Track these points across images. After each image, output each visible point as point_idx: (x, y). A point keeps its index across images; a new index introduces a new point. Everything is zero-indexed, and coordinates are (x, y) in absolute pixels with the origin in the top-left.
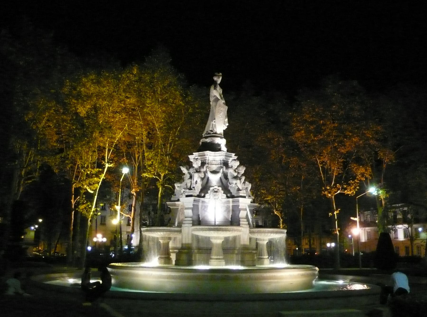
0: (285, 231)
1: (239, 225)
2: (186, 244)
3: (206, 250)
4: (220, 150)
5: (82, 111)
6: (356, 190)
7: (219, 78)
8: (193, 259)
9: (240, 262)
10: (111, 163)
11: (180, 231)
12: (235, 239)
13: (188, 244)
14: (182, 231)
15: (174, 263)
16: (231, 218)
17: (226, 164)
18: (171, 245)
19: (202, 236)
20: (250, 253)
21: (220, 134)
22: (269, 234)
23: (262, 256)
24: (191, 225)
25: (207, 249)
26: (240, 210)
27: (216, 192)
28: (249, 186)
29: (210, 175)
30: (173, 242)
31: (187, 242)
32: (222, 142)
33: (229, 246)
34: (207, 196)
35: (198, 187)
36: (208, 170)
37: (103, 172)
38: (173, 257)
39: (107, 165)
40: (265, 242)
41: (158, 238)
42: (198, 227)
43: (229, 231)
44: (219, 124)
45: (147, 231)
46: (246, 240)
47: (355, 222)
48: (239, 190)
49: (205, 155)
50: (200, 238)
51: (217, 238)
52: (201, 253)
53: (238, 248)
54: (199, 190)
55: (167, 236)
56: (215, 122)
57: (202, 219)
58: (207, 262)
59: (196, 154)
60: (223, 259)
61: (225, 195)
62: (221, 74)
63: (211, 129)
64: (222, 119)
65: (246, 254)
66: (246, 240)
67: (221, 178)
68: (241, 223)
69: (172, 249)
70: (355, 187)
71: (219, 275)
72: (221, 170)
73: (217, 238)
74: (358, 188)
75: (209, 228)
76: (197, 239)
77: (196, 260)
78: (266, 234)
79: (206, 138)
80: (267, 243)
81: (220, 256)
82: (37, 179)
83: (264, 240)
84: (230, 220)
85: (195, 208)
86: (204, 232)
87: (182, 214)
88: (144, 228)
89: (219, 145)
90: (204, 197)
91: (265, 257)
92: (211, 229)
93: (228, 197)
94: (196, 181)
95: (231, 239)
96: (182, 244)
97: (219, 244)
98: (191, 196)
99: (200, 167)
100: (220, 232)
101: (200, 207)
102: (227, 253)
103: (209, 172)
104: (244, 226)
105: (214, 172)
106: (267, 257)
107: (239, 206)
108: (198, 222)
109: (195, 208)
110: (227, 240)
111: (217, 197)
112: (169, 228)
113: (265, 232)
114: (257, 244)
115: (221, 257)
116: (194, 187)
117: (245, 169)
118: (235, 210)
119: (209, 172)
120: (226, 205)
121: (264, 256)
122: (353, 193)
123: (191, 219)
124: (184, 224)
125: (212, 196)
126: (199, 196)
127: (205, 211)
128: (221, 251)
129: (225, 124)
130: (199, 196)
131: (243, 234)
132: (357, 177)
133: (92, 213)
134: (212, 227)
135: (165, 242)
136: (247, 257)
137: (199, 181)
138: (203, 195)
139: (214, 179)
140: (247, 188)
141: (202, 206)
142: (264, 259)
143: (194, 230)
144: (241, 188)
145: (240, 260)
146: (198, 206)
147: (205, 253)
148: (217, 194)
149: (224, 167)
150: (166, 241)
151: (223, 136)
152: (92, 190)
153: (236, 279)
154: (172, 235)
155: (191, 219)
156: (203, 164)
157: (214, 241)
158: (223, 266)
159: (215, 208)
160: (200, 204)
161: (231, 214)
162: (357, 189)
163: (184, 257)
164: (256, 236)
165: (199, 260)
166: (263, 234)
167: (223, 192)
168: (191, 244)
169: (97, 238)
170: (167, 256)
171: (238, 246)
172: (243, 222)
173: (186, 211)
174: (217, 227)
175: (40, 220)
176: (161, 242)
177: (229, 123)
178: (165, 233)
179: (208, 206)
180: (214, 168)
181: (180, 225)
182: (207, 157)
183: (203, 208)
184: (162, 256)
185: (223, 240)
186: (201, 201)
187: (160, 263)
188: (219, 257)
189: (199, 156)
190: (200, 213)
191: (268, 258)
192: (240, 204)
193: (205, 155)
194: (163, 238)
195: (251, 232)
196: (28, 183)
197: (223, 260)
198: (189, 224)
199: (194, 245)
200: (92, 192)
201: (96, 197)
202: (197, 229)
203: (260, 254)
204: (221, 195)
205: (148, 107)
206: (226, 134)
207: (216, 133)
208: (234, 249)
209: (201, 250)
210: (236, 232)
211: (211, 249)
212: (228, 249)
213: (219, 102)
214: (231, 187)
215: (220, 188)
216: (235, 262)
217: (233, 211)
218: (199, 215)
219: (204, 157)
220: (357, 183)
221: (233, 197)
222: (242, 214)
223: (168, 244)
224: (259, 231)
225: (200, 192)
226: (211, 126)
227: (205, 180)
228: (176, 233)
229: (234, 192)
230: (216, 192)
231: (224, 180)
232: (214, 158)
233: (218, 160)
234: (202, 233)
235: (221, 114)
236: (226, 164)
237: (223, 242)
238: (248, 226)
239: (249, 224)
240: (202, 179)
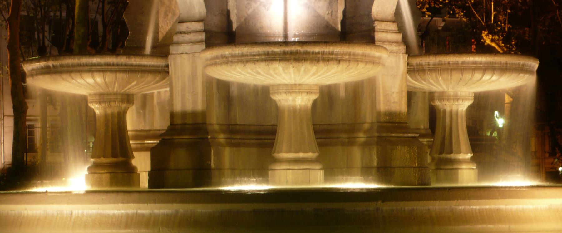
0: (535, 64)
2: (184, 115)
3: (256, 130)
8: (213, 165)
9: (374, 171)
11: (164, 72)
12: (357, 92)
13: (194, 114)
14: (171, 70)
15: (144, 182)
16: (343, 22)
18: (132, 123)
19: (242, 86)
22: (477, 75)
23: (451, 152)
24: (204, 46)
25: (259, 133)
30: (139, 113)
31: (189, 107)
33: (339, 116)
38: (142, 163)
40: (463, 106)
41: (84, 99)
42: (227, 51)
43: (339, 61)
45: (47, 71)
46: (395, 97)
50: (234, 91)
51: (295, 86)
53: (366, 126)
55: (116, 88)
57: (240, 27)
58: (261, 171)
66: (395, 97)
68: (378, 36)
69: (136, 138)
73: (295, 86)
75: (268, 54)
76: (224, 91)
77: (220, 168)
78: (467, 76)
81: (306, 152)
83: (456, 98)
84: (339, 27)
86: (250, 66)
87: (166, 15)
88: (32, 61)
90: (10, 21)
91: (461, 156)
92: (274, 54)
96: (172, 115)
97: (303, 110)
100: (304, 67)
106: (469, 156)
110: (327, 95)
112: (122, 60)
113: (462, 69)
114: (434, 115)
115: (310, 155)
121: (459, 152)
123: (199, 26)
124: (178, 43)
128: (308, 134)
131: (385, 73)
134: (277, 49)
135: (109, 111)
136: (402, 155)
143: (214, 62)
145: (375, 163)
150: (114, 108)
154: (137, 86)
155: (199, 26)
157: (285, 100)
158: (317, 180)
163: (181, 159)
166: (456, 76)
168: (204, 114)
170: (120, 159)
171: (368, 118)
172: (385, 33)
174: (290, 51)
176: (97, 112)
178: (109, 77)
181: (162, 49)
184: (103, 160)
185: (314, 97)
188: (301, 155)
191: (473, 160)
194: (103, 98)
195: (411, 70)
197: (318, 166)
198: (195, 42)
199: (215, 119)
202: (223, 57)
208: (352, 128)
209: (236, 134)
210: (361, 66)
212: (333, 127)
218: (228, 13)
223: (121, 118)
224: (440, 64)
228: (149, 78)
234: (245, 74)
237: (315, 103)
238: (403, 48)
239: (405, 41)
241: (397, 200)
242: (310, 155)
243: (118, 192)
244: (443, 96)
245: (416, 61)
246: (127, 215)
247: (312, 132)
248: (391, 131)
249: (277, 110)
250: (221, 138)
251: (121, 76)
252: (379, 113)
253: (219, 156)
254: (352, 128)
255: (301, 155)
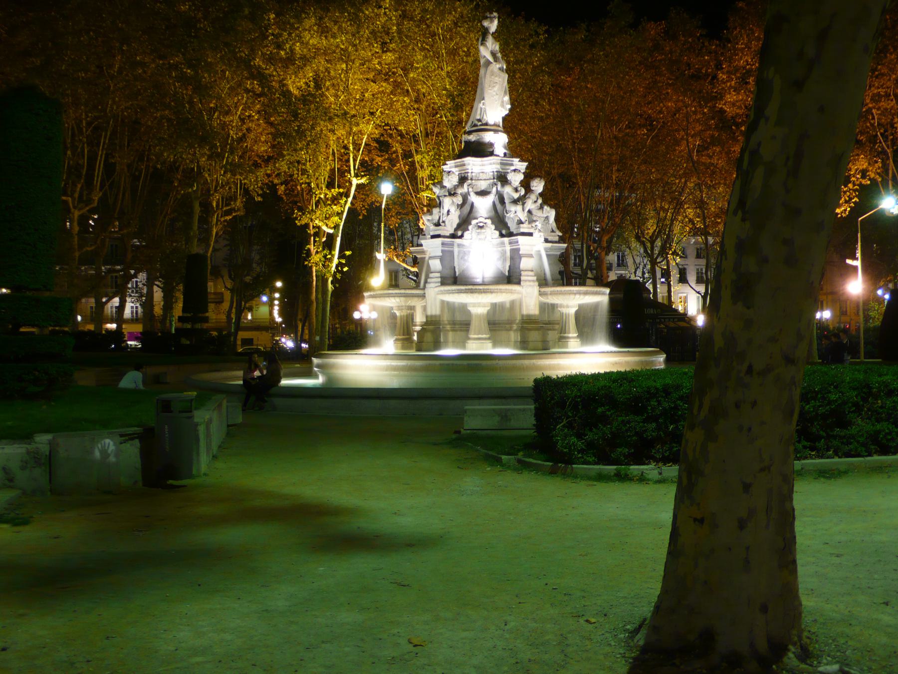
0: (608, 291)
1: (519, 283)
2: (431, 316)
3: (462, 324)
4: (492, 154)
5: (296, 84)
6: (852, 205)
7: (492, 22)
10: (362, 176)
11: (423, 296)
13: (435, 316)
17: (502, 179)
20: (541, 331)
21: (495, 125)
26: (520, 257)
27: (481, 227)
28: (552, 214)
29: (473, 198)
31: (434, 313)
32: (499, 141)
34: (466, 234)
35: (452, 221)
36: (470, 190)
39: (355, 181)
40: (572, 311)
41: (392, 308)
43: (492, 292)
44: (494, 106)
47: (856, 268)
48: (520, 222)
49: (464, 165)
51: (478, 305)
54: (455, 226)
59: (451, 163)
60: (489, 339)
61: (497, 233)
63: (478, 117)
64: (496, 97)
68: (522, 278)
70: (851, 199)
72: (494, 189)
73: (478, 305)
79: (470, 133)
82: (241, 213)
83: (568, 307)
89: (491, 145)
90: (461, 237)
91: (570, 335)
93: (502, 235)
94: (448, 211)
95: (508, 305)
98: (438, 236)
99: (456, 187)
100: (476, 295)
101: (456, 254)
102: (495, 330)
103: (472, 194)
104: (528, 283)
105: (483, 193)
106: (576, 335)
107: (518, 250)
108: (454, 279)
109: (447, 257)
110: (495, 308)
111: (482, 236)
112: (403, 291)
113: (571, 293)
115: (484, 336)
116: (444, 222)
118: (515, 256)
119: (472, 194)
120: (500, 249)
122: (845, 210)
123: (438, 275)
125: (474, 235)
126: (453, 236)
128: (485, 326)
129: (503, 106)
130: (453, 236)
131: (528, 297)
132: (853, 179)
133: (333, 269)
137: (453, 209)
138: (460, 233)
139: (483, 206)
140: (547, 218)
141: (459, 252)
142: (568, 338)
143: (443, 293)
144: (523, 220)
146: (452, 252)
148: (483, 231)
149: (499, 184)
152: (331, 228)
156: (463, 179)
159: (482, 254)
160: (456, 250)
161: (508, 264)
162: (854, 203)
163: (429, 337)
164: (551, 300)
167: (493, 227)
169: (361, 312)
173: (431, 262)
175: (279, 284)
179: (469, 252)
180: (483, 185)
182: (469, 167)
183: (461, 255)
186: (456, 245)
187: (397, 348)
188: (480, 336)
189: (456, 166)
190: (456, 264)
192: (521, 247)
193: (464, 165)
194: (400, 308)
195: (541, 294)
199: (446, 318)
200: (331, 231)
203: (563, 330)
204: (491, 232)
205: (418, 68)
206: (509, 125)
207: (486, 124)
212: (496, 324)
213: (491, 67)
214: (509, 218)
215: (489, 222)
216: (512, 343)
217: (512, 258)
219: (465, 167)
220: (855, 191)
221: (511, 234)
222: (526, 264)
225: (456, 230)
226: (479, 112)
227: (467, 208)
228: (416, 299)
229: (513, 227)
230: (481, 227)
231: (499, 206)
235: (496, 89)
236: (502, 179)
237: (488, 312)
240: (461, 207)
242: (484, 336)
243: (628, 352)
244: (562, 306)
245: (543, 290)
247: (486, 325)
248: (529, 324)
252: (523, 316)
253: (446, 337)
254: (510, 322)
255: (480, 336)
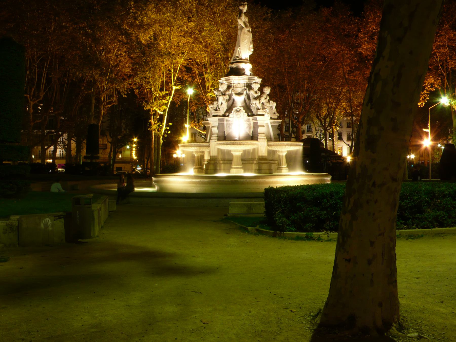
0: (302, 144)
1: (257, 139)
2: (213, 156)
3: (228, 160)
4: (244, 74)
5: (144, 38)
6: (426, 101)
7: (244, 7)
10: (178, 85)
11: (209, 146)
13: (215, 156)
16: (252, 134)
20: (268, 164)
21: (245, 59)
26: (258, 127)
27: (238, 111)
28: (274, 105)
29: (234, 97)
31: (214, 155)
32: (247, 67)
34: (231, 115)
35: (224, 108)
36: (233, 92)
37: (170, 95)
39: (174, 88)
40: (284, 154)
41: (193, 152)
43: (243, 144)
44: (245, 50)
47: (427, 133)
48: (258, 109)
49: (230, 80)
51: (237, 151)
52: (225, 164)
54: (225, 111)
56: (240, 49)
57: (227, 135)
58: (229, 171)
60: (242, 168)
61: (246, 114)
62: (246, 3)
63: (237, 56)
65: (263, 163)
67: (245, 99)
68: (259, 137)
70: (425, 98)
71: (230, 180)
72: (245, 92)
73: (237, 151)
74: (428, 98)
79: (233, 63)
80: (286, 155)
83: (282, 152)
85: (221, 126)
89: (243, 70)
90: (228, 116)
91: (283, 166)
93: (249, 116)
94: (222, 103)
98: (216, 116)
99: (225, 91)
102: (245, 164)
103: (234, 94)
104: (262, 140)
105: (239, 94)
108: (224, 137)
109: (221, 126)
113: (283, 145)
115: (239, 167)
116: (219, 109)
117: (270, 89)
119: (234, 94)
122: (422, 104)
123: (216, 135)
126: (224, 116)
127: (230, 128)
129: (249, 50)
130: (224, 116)
131: (262, 147)
138: (227, 114)
139: (239, 100)
141: (227, 124)
142: (282, 168)
144: (260, 108)
146: (223, 124)
147: (228, 164)
148: (239, 113)
149: (247, 89)
151: (249, 61)
152: (162, 111)
153: (243, 183)
156: (229, 87)
159: (238, 125)
160: (225, 123)
162: (427, 100)
163: (211, 167)
165: (224, 169)
166: (282, 147)
167: (244, 111)
168: (217, 156)
177: (254, 49)
178: (196, 148)
180: (239, 90)
183: (228, 126)
184: (198, 167)
185: (242, 152)
186: (225, 120)
187: (195, 172)
188: (237, 167)
189: (226, 80)
193: (230, 80)
194: (197, 152)
195: (268, 145)
196: (108, 107)
199: (220, 157)
200: (162, 113)
201: (166, 117)
203: (279, 164)
204: (243, 114)
207: (241, 59)
211: (232, 161)
212: (246, 160)
213: (243, 30)
214: (252, 107)
215: (242, 108)
216: (254, 170)
217: (254, 127)
221: (253, 115)
225: (225, 112)
226: (237, 53)
227: (231, 102)
228: (205, 148)
230: (238, 111)
231: (247, 101)
232: (238, 81)
233: (244, 81)
235: (246, 41)
236: (249, 86)
241: (256, 178)
242: (239, 167)
244: (279, 151)
245: (269, 143)
246: (200, 181)
247: (241, 160)
249: (232, 155)
250: (221, 162)
251: (198, 147)
252: (259, 156)
254: (253, 160)
